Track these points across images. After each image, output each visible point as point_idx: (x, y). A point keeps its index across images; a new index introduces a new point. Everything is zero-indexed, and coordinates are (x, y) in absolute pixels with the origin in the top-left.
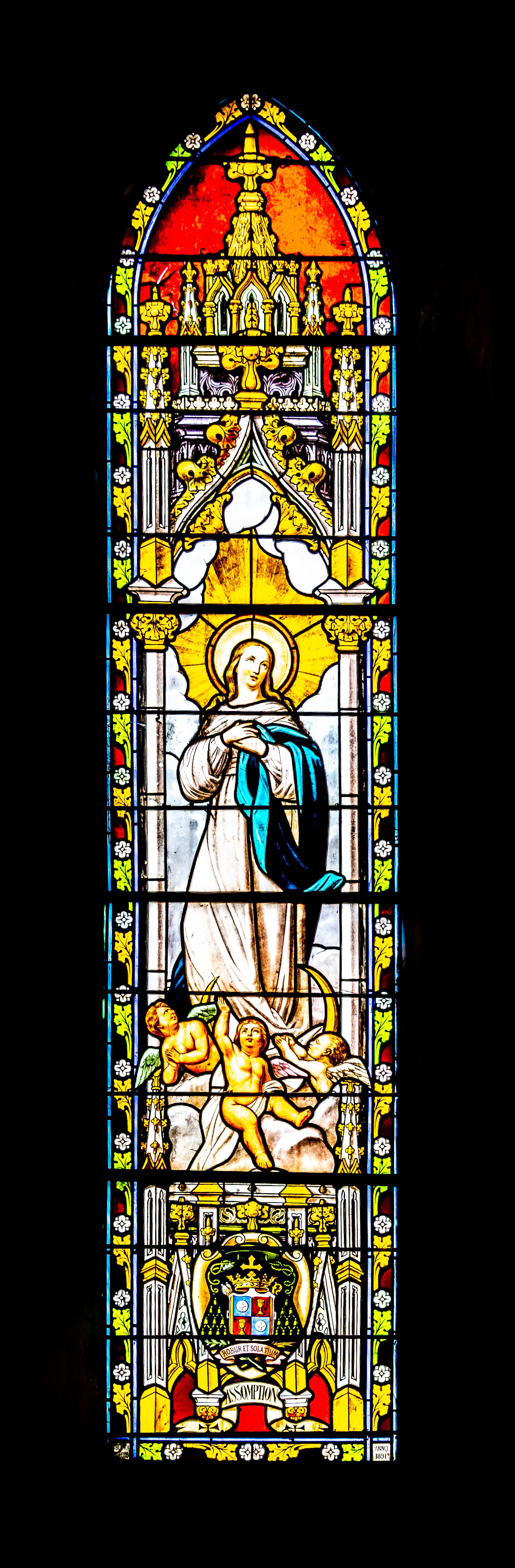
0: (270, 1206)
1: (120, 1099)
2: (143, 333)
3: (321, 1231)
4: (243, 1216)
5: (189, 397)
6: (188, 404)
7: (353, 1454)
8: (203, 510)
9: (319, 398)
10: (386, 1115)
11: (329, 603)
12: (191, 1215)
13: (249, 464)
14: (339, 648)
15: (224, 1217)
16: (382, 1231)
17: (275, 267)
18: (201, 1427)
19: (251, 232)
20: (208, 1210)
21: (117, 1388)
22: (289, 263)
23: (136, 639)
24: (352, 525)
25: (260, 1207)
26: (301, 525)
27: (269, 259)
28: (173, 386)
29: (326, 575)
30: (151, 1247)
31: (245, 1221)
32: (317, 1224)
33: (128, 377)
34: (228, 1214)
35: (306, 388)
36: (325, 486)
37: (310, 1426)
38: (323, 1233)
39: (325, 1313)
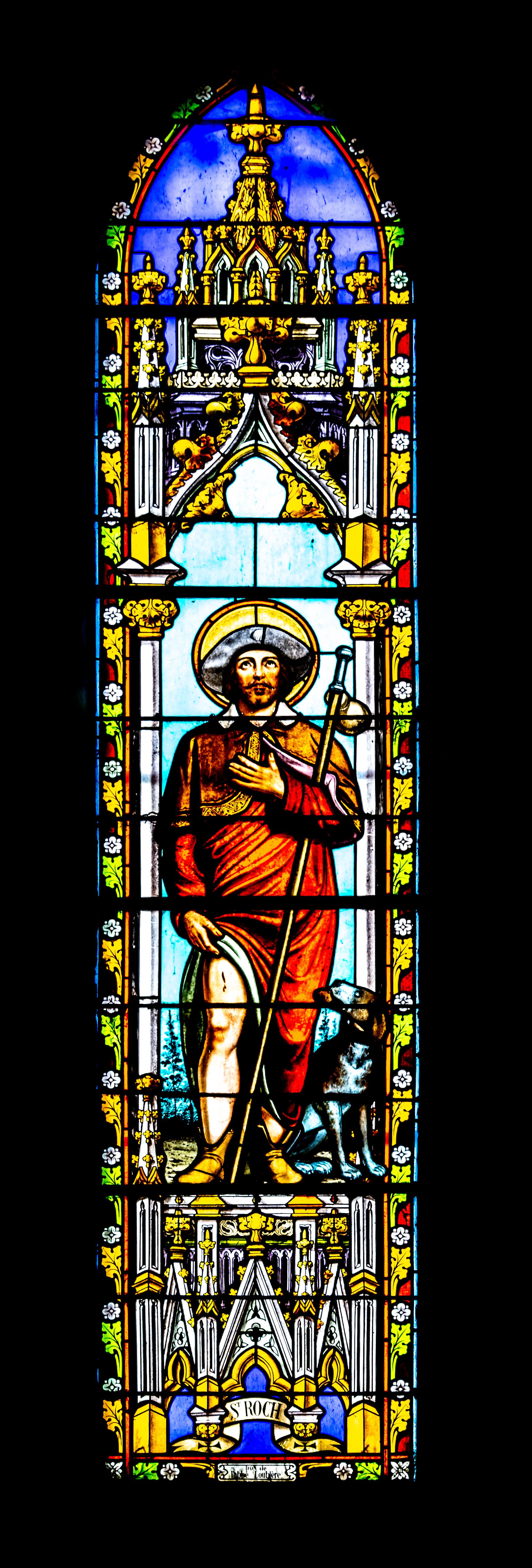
0: (276, 1218)
1: (109, 395)
3: (332, 1242)
4: (245, 1228)
7: (370, 1471)
9: (332, 372)
13: (253, 442)
14: (354, 635)
15: (224, 1229)
17: (282, 233)
18: (200, 1446)
21: (107, 632)
22: (298, 230)
25: (264, 1218)
26: (311, 503)
29: (339, 557)
30: (143, 1394)
31: (248, 1234)
32: (329, 1235)
33: (118, 489)
34: (229, 1227)
35: (318, 361)
36: (337, 465)
38: (335, 1245)
39: (336, 1326)
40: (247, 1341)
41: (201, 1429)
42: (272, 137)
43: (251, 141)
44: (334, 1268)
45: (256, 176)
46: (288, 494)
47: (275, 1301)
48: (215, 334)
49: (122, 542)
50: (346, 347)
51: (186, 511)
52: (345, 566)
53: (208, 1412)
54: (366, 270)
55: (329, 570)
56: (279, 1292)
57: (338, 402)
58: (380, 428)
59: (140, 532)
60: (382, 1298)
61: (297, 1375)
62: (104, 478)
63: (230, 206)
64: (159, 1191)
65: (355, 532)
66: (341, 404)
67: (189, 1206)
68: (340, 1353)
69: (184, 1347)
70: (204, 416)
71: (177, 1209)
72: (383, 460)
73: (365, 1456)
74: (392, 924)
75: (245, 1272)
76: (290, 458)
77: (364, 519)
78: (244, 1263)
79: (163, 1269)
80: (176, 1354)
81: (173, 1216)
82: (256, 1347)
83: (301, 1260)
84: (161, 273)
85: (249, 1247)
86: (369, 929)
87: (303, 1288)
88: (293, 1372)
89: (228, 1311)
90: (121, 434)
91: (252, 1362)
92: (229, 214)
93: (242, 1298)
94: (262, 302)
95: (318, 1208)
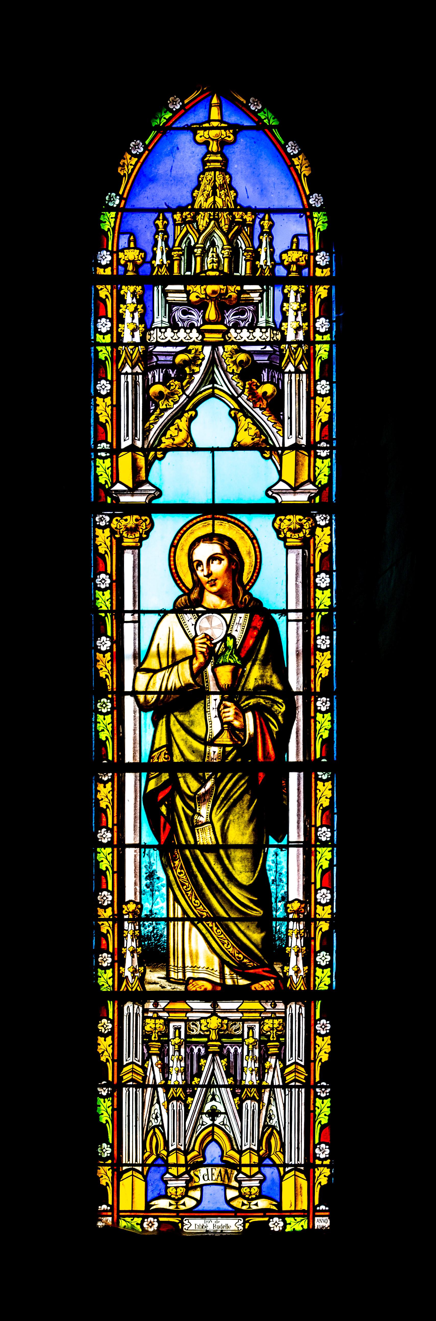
0: (229, 1020)
1: (103, 924)
2: (121, 273)
4: (206, 1029)
5: (160, 328)
6: (159, 334)
8: (172, 424)
10: (326, 869)
11: (280, 501)
12: (162, 1028)
13: (211, 386)
14: (287, 544)
16: (323, 902)
17: (234, 217)
18: (170, 1205)
19: (214, 188)
20: (177, 1024)
22: (246, 214)
23: (115, 538)
24: (299, 434)
25: (220, 1020)
27: (231, 211)
28: (146, 319)
31: (208, 1033)
32: (269, 1033)
36: (275, 406)
37: (263, 1204)
38: (273, 1041)
40: (207, 1120)
41: (171, 1191)
42: (227, 138)
43: (211, 142)
44: (272, 1061)
45: (215, 170)
46: (237, 427)
47: (228, 1089)
48: (182, 297)
49: (112, 471)
50: (282, 306)
51: (160, 442)
52: (282, 486)
53: (177, 1178)
54: (298, 249)
55: (269, 489)
56: (231, 1081)
57: (275, 351)
58: (308, 372)
59: (125, 461)
60: (309, 1086)
61: (244, 1148)
62: (99, 419)
63: (194, 194)
64: (141, 997)
65: (289, 458)
66: (278, 353)
67: (164, 1010)
68: (276, 1130)
69: (159, 1125)
70: (173, 366)
71: (154, 1012)
72: (310, 403)
73: (294, 1213)
74: (315, 639)
75: (206, 1064)
76: (239, 399)
77: (295, 447)
78: (205, 1057)
79: (144, 1061)
80: (152, 1132)
81: (151, 1018)
82: (213, 1125)
83: (248, 1055)
84: (141, 251)
85: (210, 1043)
86: (298, 827)
87: (250, 1078)
88: (241, 1146)
89: (193, 1095)
90: (111, 383)
91: (210, 1138)
92: (194, 199)
93: (202, 1086)
94: (217, 273)
95: (261, 1013)
